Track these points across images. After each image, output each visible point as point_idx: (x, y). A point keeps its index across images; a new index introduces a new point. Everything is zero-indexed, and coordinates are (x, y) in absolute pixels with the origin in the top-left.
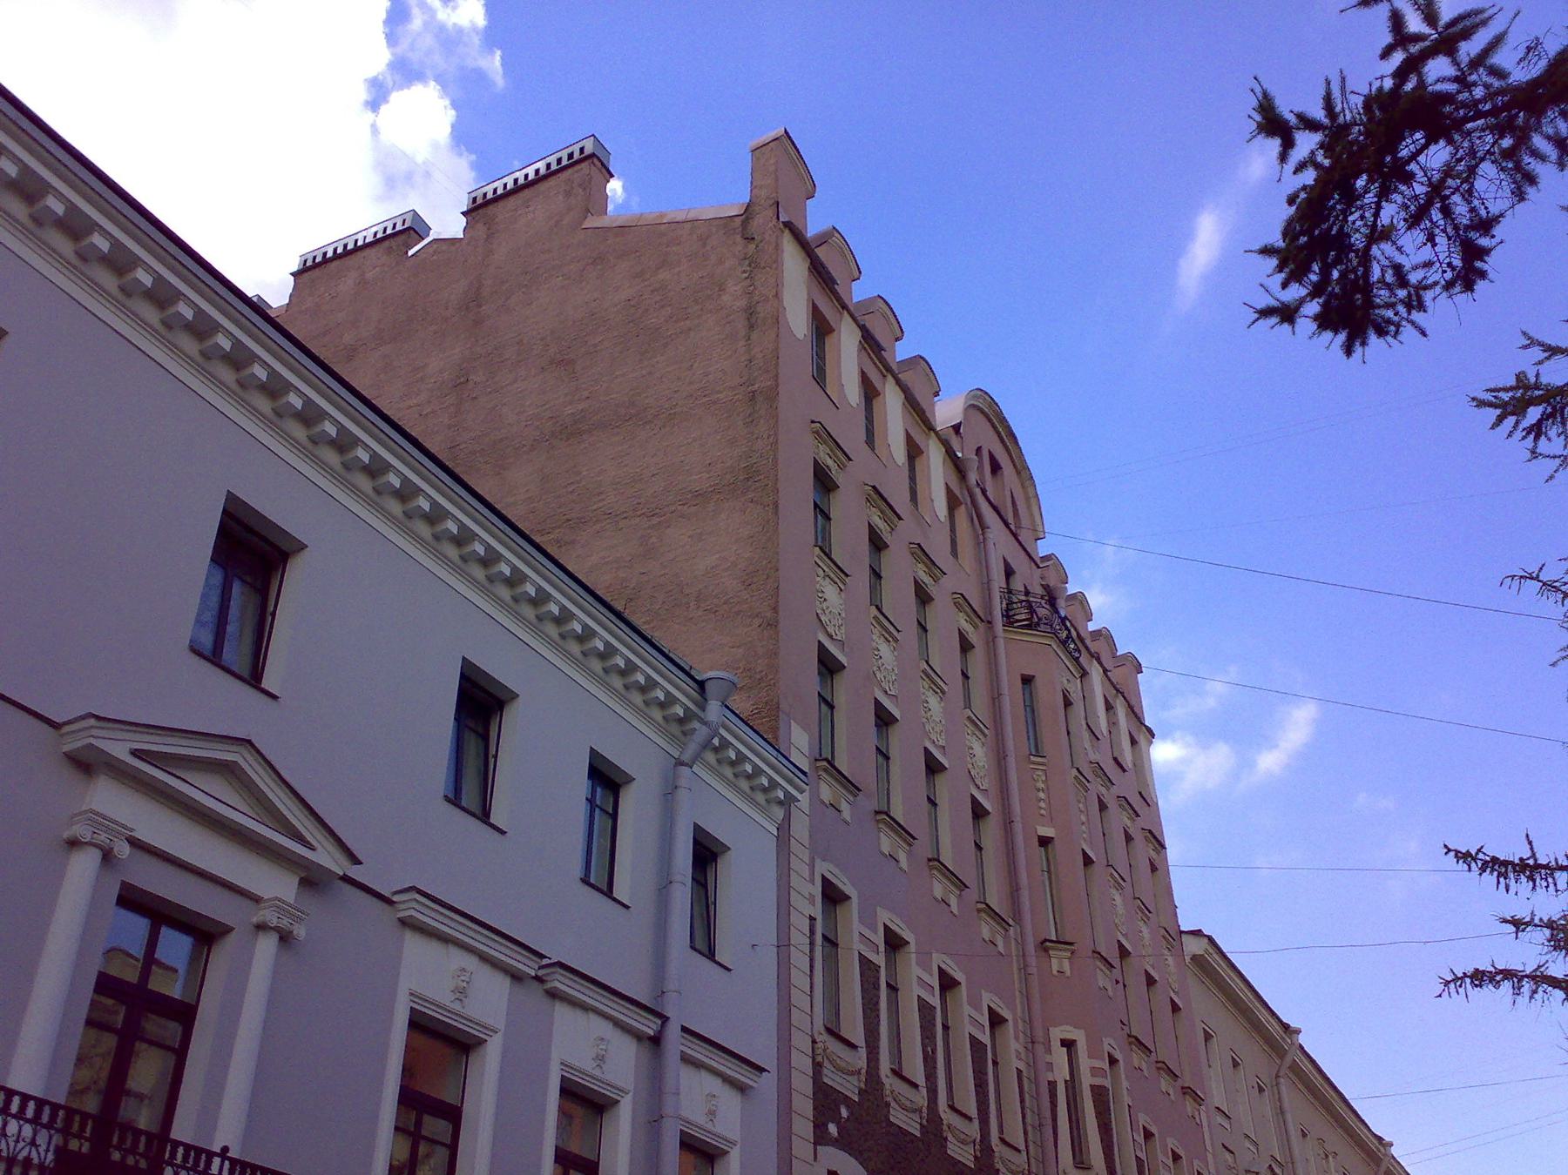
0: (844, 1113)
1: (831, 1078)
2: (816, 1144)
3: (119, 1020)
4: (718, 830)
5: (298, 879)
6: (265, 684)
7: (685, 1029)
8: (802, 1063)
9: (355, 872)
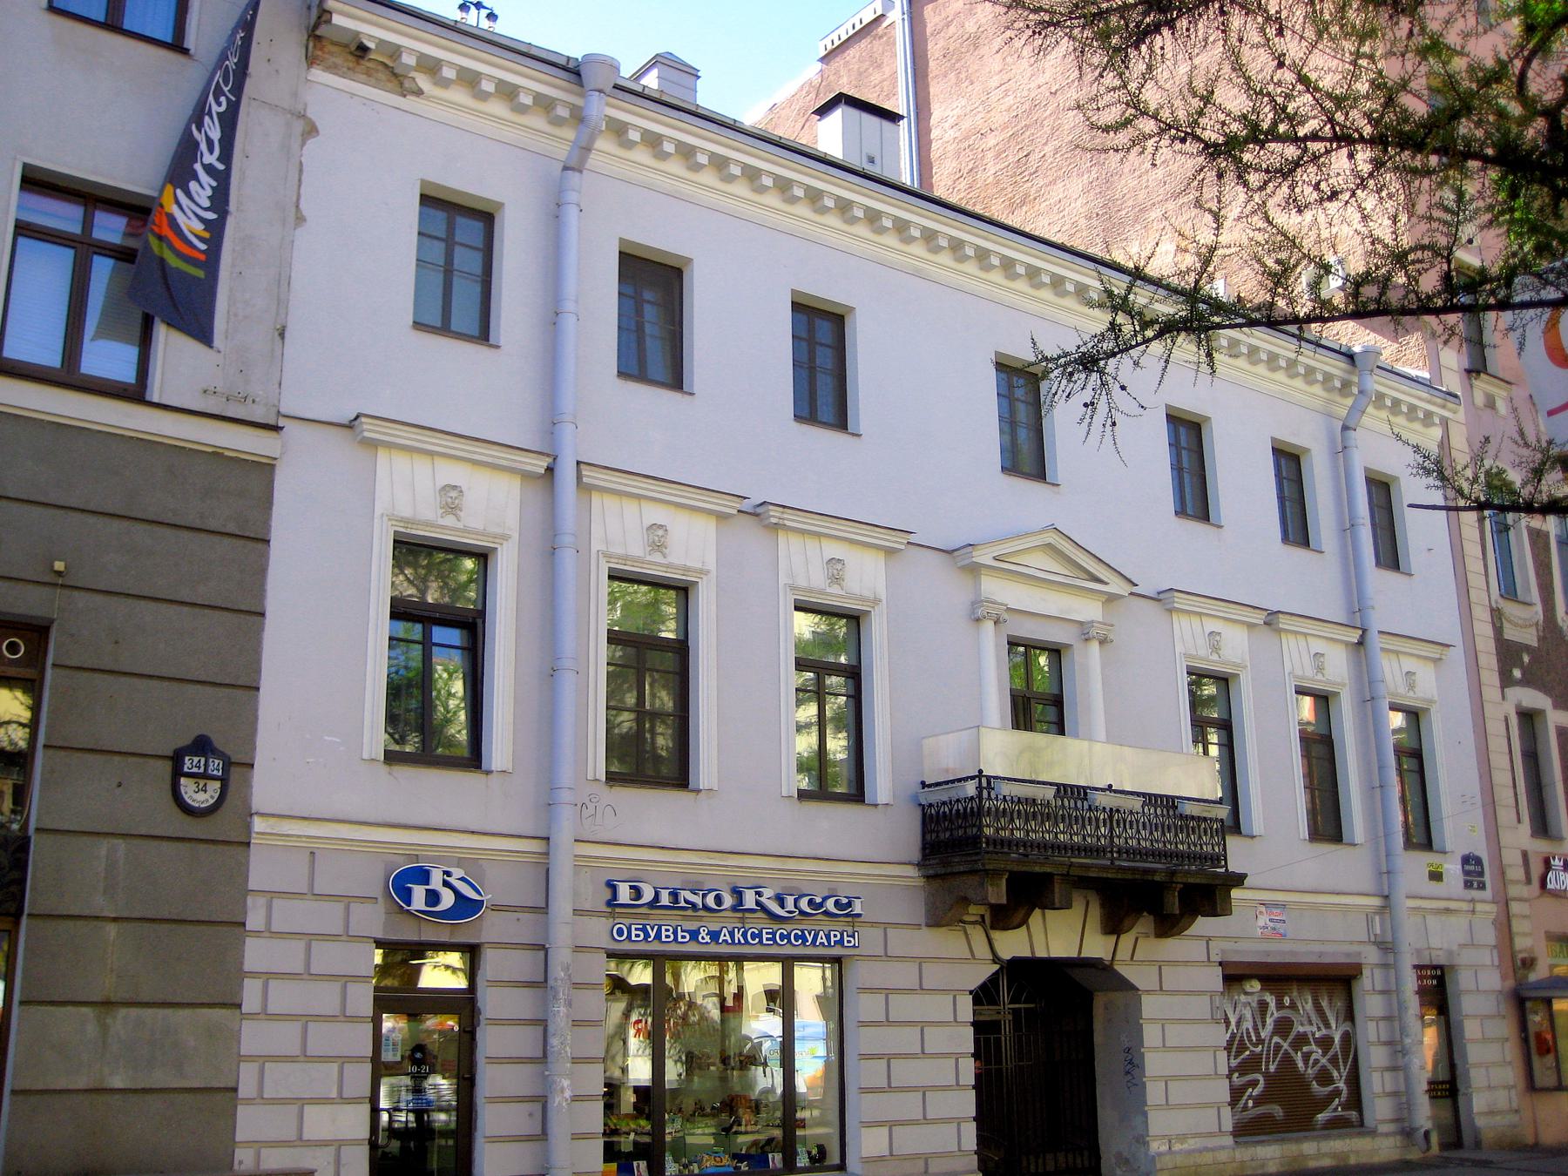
0: (1526, 659)
1: (1510, 633)
2: (1502, 688)
3: (418, 637)
4: (661, 238)
5: (1100, 603)
6: (453, 328)
7: (1380, 632)
8: (1484, 630)
9: (1135, 590)
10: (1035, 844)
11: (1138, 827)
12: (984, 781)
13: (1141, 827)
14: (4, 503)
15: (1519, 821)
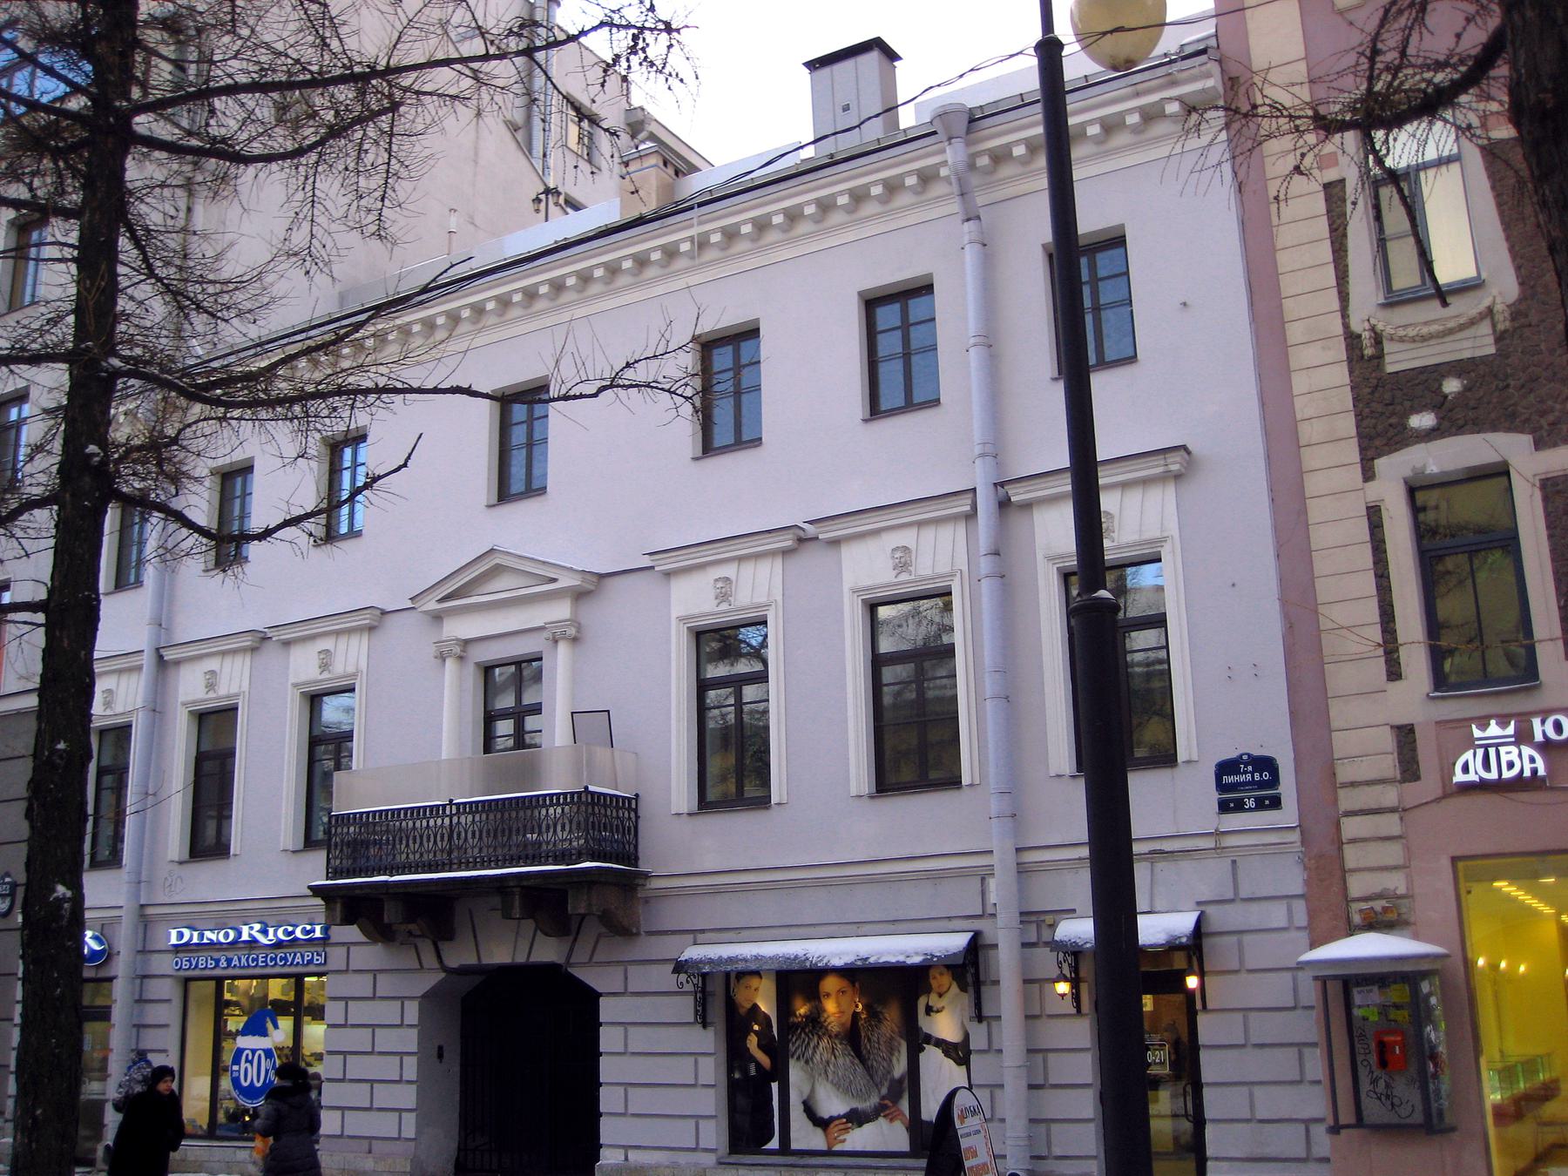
10: (339, 870)
11: (408, 841)
12: (454, 807)
13: (463, 834)
14: (2, 763)
15: (1394, 673)
